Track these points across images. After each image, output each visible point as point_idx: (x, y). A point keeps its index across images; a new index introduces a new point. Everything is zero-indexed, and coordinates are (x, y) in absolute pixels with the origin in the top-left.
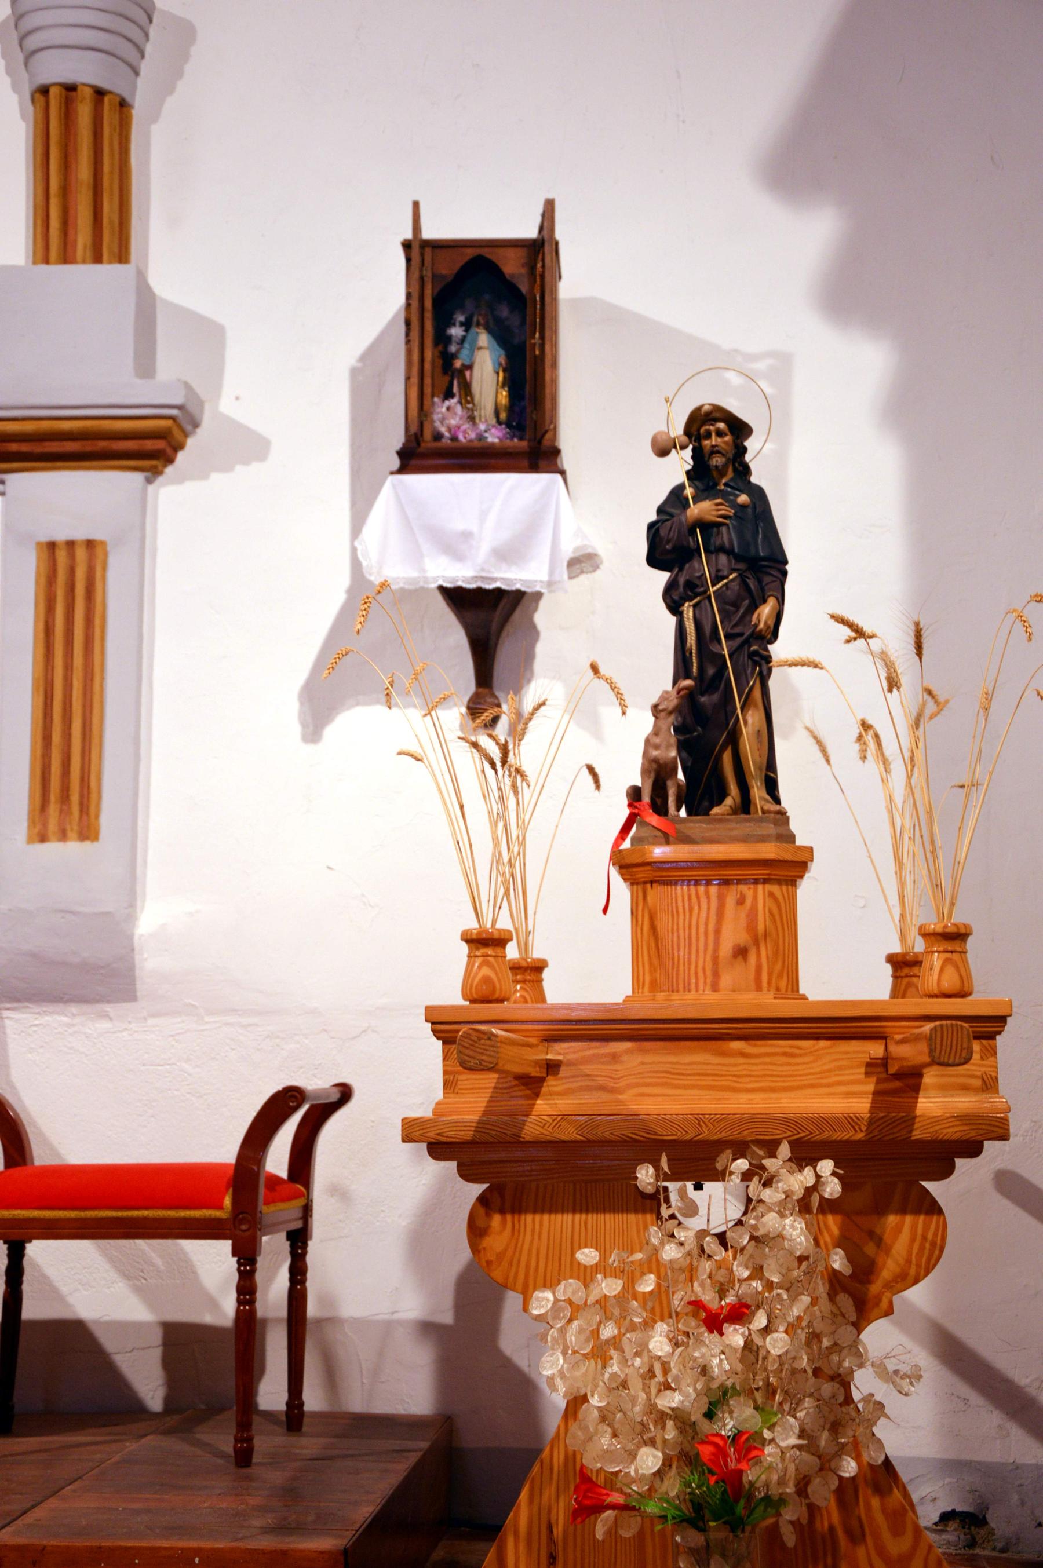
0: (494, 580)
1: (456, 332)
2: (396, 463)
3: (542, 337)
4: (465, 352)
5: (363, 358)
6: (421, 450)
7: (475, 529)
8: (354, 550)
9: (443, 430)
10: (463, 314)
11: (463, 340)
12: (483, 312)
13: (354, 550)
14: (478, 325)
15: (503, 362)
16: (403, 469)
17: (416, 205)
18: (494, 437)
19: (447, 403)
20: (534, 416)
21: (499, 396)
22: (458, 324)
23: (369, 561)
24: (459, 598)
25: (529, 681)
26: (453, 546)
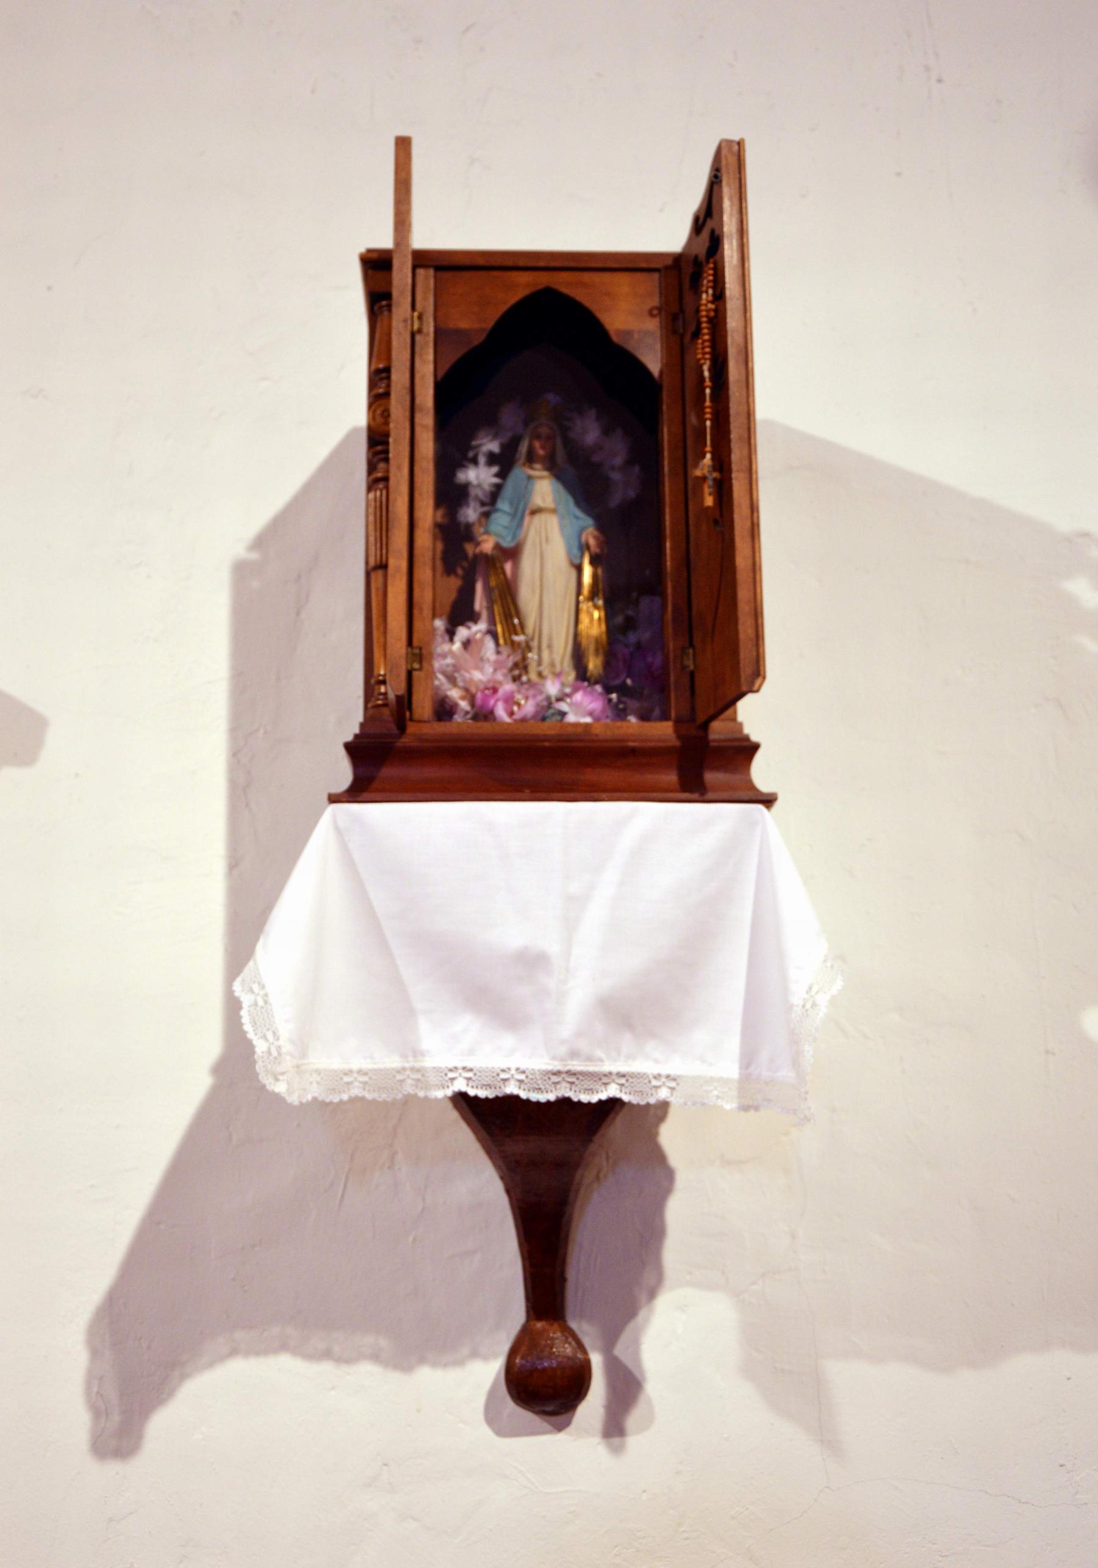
0: (603, 1078)
1: (478, 476)
2: (343, 774)
3: (722, 464)
4: (500, 521)
5: (260, 542)
6: (405, 741)
7: (553, 948)
8: (233, 1006)
9: (454, 694)
10: (495, 436)
11: (495, 493)
12: (544, 431)
13: (233, 1006)
14: (531, 459)
15: (592, 542)
16: (360, 790)
17: (403, 145)
18: (582, 709)
19: (462, 633)
20: (690, 664)
21: (584, 619)
22: (482, 460)
23: (275, 1035)
24: (497, 1119)
25: (652, 1294)
26: (492, 990)
